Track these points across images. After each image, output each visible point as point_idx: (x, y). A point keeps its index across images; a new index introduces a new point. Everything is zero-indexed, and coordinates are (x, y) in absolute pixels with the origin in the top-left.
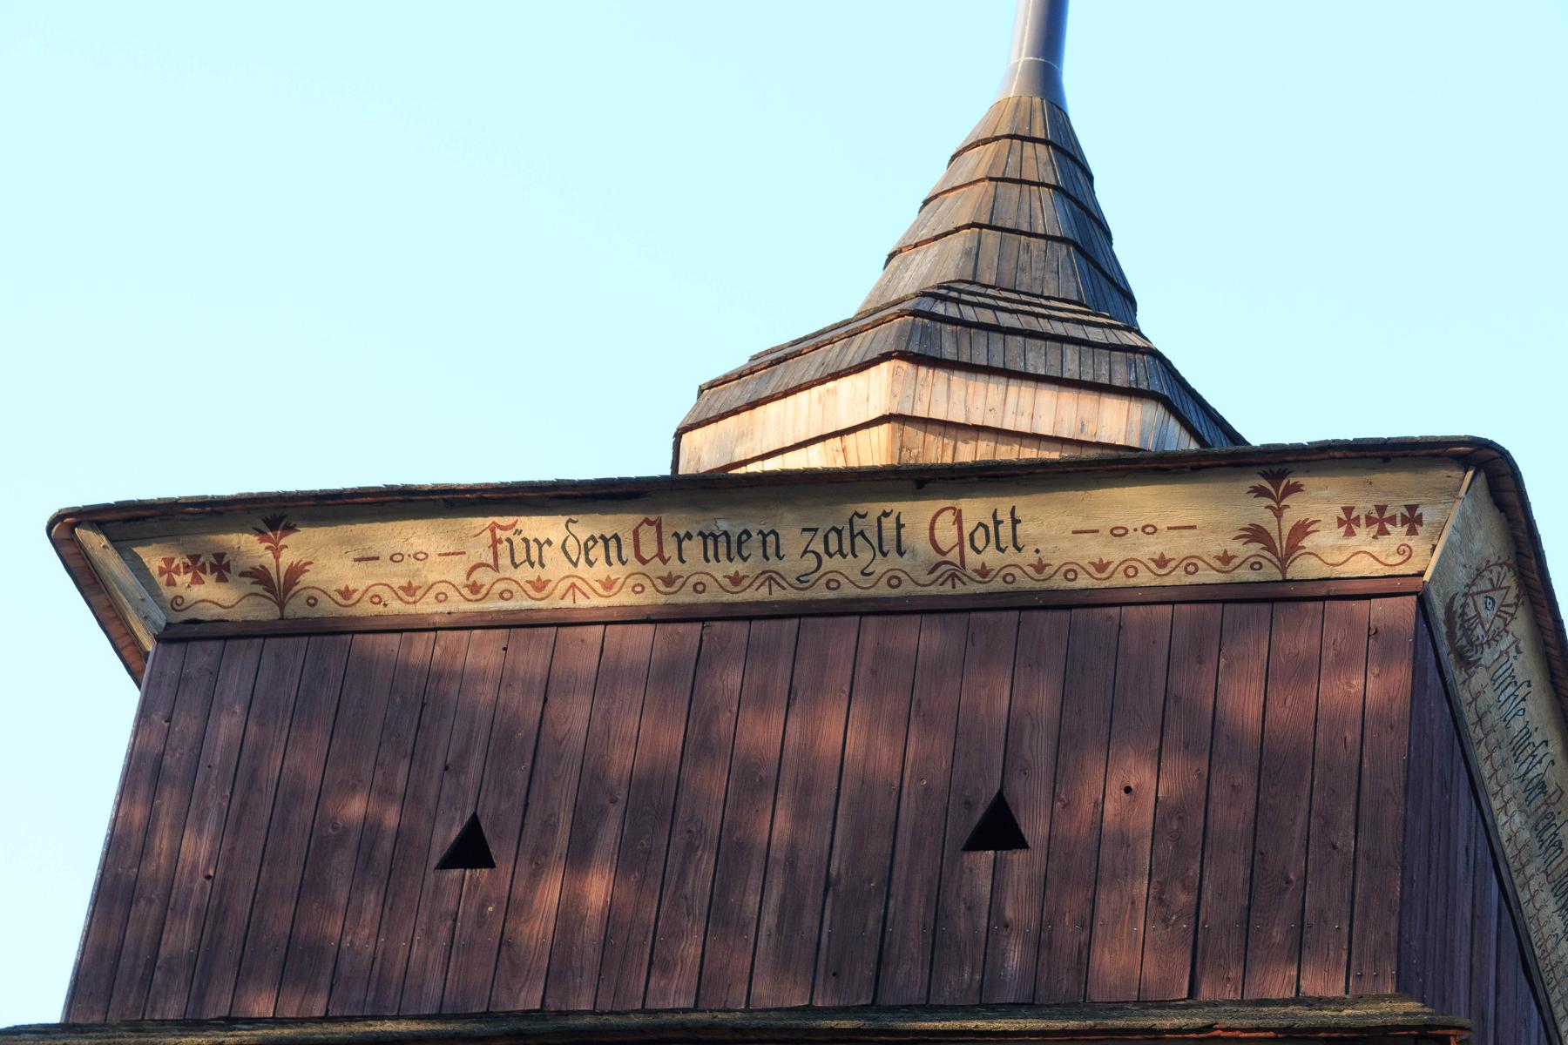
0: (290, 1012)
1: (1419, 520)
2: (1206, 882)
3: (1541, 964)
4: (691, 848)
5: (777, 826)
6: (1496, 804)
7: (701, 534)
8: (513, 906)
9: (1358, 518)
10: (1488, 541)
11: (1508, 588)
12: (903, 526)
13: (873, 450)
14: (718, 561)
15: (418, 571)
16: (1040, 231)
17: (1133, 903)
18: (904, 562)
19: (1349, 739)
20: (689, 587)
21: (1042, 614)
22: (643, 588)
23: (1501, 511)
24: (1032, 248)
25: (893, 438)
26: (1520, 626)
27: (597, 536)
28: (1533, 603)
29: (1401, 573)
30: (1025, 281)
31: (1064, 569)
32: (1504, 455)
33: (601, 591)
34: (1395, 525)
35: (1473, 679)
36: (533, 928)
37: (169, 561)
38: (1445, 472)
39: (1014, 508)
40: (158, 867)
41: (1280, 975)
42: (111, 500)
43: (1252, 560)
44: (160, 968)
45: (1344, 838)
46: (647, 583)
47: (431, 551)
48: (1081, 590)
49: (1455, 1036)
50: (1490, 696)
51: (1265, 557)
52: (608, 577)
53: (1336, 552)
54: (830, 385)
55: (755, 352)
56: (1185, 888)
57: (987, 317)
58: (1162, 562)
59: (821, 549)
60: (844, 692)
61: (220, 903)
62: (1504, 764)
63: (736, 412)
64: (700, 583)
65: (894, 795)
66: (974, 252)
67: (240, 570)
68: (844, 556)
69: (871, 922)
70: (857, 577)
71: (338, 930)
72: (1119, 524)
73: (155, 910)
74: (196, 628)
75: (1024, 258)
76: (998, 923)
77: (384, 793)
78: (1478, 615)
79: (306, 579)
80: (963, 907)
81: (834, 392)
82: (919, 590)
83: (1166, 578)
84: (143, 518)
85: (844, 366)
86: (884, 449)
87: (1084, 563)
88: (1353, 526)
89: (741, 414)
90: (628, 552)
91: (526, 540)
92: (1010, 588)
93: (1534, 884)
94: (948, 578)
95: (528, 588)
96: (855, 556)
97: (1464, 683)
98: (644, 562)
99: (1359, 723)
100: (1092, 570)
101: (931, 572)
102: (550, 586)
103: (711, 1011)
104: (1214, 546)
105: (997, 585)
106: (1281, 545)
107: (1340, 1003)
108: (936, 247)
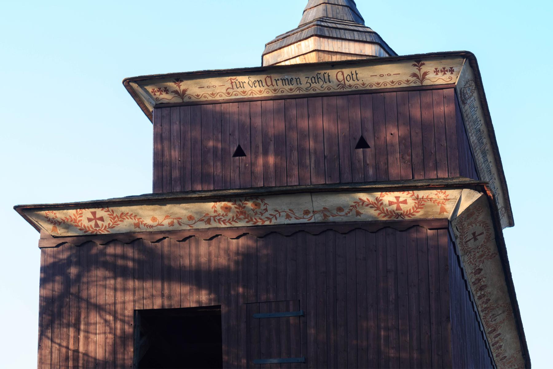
0: (206, 189)
1: (453, 71)
2: (413, 154)
3: (479, 169)
4: (291, 150)
5: (311, 145)
6: (470, 135)
7: (281, 79)
8: (252, 164)
9: (439, 71)
10: (469, 75)
11: (473, 86)
12: (330, 76)
13: (312, 59)
14: (286, 85)
15: (214, 90)
16: (340, 4)
17: (396, 159)
18: (330, 84)
19: (442, 121)
20: (280, 91)
21: (365, 95)
22: (269, 92)
23: (472, 68)
24: (339, 8)
25: (317, 55)
26: (475, 95)
27: (256, 80)
28: (478, 89)
29: (450, 83)
30: (339, 16)
31: (369, 84)
32: (472, 55)
33: (259, 93)
34: (448, 72)
35: (466, 107)
36: (258, 169)
37: (154, 90)
38: (459, 59)
39: (356, 71)
40: (167, 159)
41: (433, 173)
42: (137, 76)
43: (414, 81)
44: (173, 181)
45: (444, 143)
46: (270, 91)
47: (216, 85)
48: (374, 89)
49: (485, 185)
50: (469, 110)
51: (417, 80)
52: (260, 90)
53: (434, 79)
54: (299, 43)
55: (277, 36)
56: (408, 155)
57: (334, 25)
58: (393, 82)
59: (310, 82)
60: (321, 114)
61: (183, 166)
62: (472, 126)
63: (276, 50)
64: (282, 91)
65: (337, 137)
66: (326, 9)
67: (171, 91)
68: (316, 83)
69: (336, 165)
70: (320, 88)
71: (213, 170)
72: (382, 74)
73: (168, 168)
74: (163, 105)
75: (338, 11)
76: (366, 165)
77: (217, 140)
78: (467, 92)
79: (187, 93)
80: (357, 161)
81: (300, 45)
82: (335, 91)
83: (394, 86)
84: (146, 80)
85: (302, 38)
86: (314, 58)
87: (374, 83)
88: (438, 73)
89: (278, 51)
90: (264, 84)
91: (239, 82)
92: (357, 89)
93: (477, 152)
94: (342, 88)
95: (241, 93)
96: (319, 83)
97: (464, 108)
98: (268, 86)
99: (444, 117)
100: (376, 85)
101: (338, 86)
102: (246, 92)
103: (305, 185)
104: (405, 78)
105: (354, 89)
106: (421, 77)
107: (447, 179)
108: (315, 9)
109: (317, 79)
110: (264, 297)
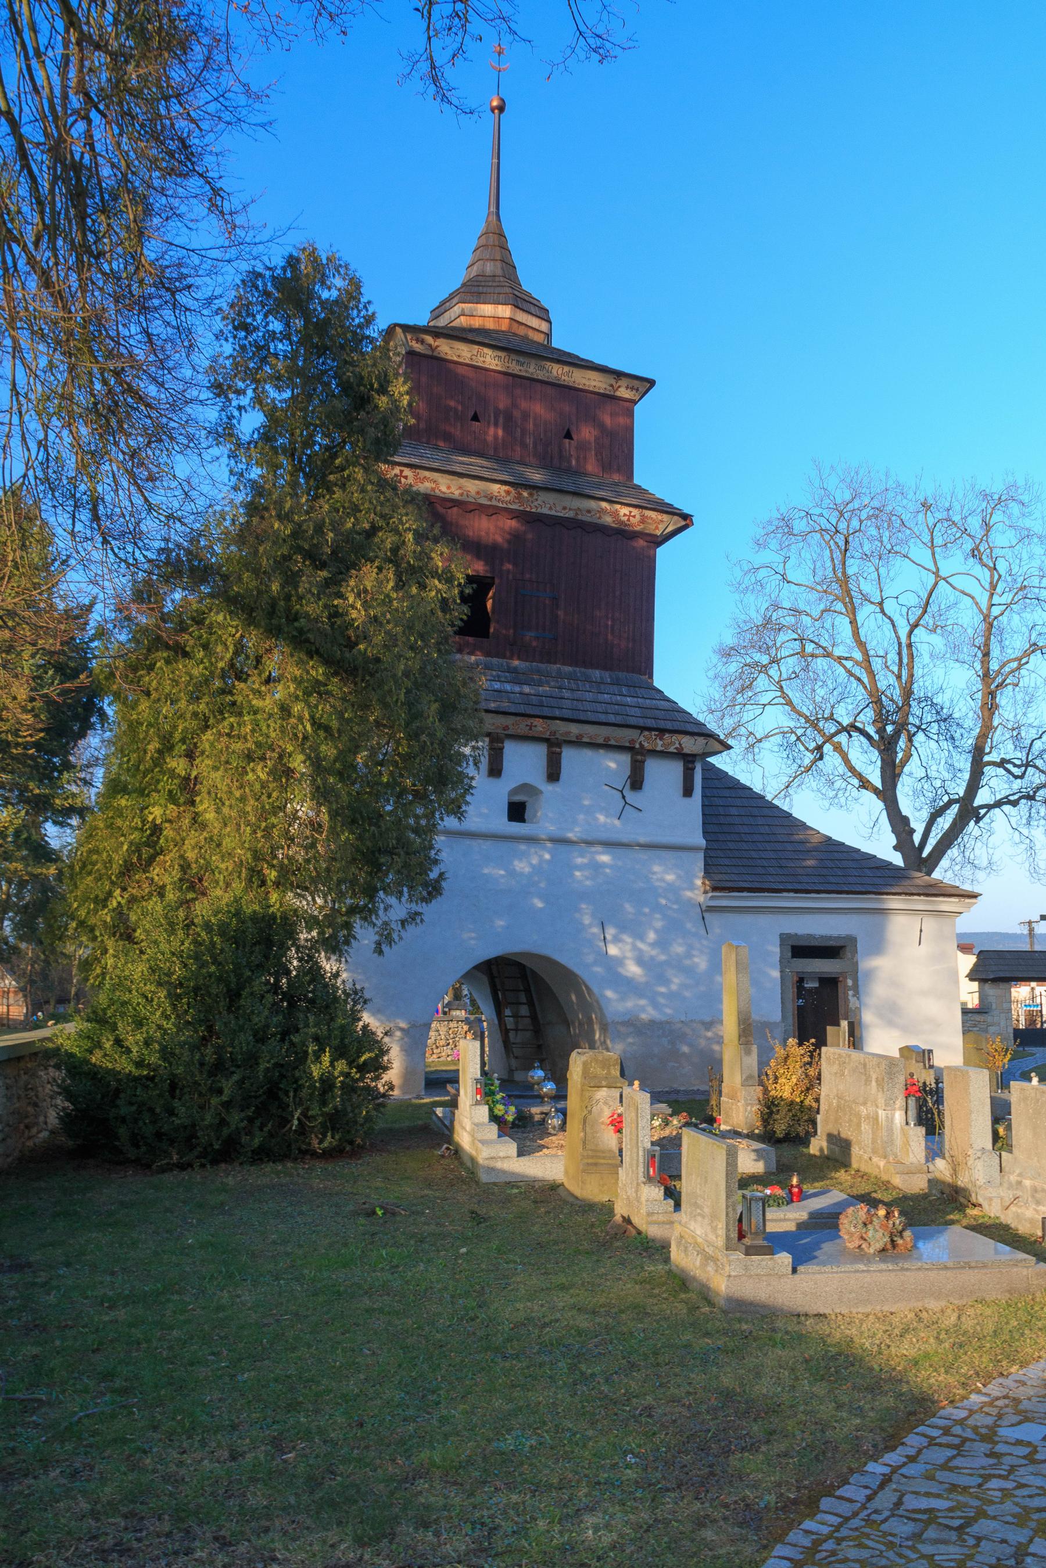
104: (604, 386)
109: (543, 368)
110: (528, 576)
